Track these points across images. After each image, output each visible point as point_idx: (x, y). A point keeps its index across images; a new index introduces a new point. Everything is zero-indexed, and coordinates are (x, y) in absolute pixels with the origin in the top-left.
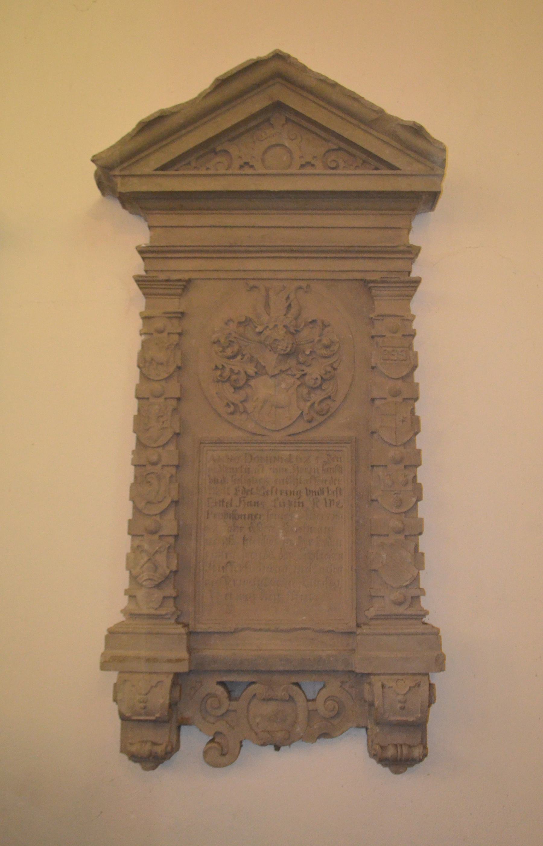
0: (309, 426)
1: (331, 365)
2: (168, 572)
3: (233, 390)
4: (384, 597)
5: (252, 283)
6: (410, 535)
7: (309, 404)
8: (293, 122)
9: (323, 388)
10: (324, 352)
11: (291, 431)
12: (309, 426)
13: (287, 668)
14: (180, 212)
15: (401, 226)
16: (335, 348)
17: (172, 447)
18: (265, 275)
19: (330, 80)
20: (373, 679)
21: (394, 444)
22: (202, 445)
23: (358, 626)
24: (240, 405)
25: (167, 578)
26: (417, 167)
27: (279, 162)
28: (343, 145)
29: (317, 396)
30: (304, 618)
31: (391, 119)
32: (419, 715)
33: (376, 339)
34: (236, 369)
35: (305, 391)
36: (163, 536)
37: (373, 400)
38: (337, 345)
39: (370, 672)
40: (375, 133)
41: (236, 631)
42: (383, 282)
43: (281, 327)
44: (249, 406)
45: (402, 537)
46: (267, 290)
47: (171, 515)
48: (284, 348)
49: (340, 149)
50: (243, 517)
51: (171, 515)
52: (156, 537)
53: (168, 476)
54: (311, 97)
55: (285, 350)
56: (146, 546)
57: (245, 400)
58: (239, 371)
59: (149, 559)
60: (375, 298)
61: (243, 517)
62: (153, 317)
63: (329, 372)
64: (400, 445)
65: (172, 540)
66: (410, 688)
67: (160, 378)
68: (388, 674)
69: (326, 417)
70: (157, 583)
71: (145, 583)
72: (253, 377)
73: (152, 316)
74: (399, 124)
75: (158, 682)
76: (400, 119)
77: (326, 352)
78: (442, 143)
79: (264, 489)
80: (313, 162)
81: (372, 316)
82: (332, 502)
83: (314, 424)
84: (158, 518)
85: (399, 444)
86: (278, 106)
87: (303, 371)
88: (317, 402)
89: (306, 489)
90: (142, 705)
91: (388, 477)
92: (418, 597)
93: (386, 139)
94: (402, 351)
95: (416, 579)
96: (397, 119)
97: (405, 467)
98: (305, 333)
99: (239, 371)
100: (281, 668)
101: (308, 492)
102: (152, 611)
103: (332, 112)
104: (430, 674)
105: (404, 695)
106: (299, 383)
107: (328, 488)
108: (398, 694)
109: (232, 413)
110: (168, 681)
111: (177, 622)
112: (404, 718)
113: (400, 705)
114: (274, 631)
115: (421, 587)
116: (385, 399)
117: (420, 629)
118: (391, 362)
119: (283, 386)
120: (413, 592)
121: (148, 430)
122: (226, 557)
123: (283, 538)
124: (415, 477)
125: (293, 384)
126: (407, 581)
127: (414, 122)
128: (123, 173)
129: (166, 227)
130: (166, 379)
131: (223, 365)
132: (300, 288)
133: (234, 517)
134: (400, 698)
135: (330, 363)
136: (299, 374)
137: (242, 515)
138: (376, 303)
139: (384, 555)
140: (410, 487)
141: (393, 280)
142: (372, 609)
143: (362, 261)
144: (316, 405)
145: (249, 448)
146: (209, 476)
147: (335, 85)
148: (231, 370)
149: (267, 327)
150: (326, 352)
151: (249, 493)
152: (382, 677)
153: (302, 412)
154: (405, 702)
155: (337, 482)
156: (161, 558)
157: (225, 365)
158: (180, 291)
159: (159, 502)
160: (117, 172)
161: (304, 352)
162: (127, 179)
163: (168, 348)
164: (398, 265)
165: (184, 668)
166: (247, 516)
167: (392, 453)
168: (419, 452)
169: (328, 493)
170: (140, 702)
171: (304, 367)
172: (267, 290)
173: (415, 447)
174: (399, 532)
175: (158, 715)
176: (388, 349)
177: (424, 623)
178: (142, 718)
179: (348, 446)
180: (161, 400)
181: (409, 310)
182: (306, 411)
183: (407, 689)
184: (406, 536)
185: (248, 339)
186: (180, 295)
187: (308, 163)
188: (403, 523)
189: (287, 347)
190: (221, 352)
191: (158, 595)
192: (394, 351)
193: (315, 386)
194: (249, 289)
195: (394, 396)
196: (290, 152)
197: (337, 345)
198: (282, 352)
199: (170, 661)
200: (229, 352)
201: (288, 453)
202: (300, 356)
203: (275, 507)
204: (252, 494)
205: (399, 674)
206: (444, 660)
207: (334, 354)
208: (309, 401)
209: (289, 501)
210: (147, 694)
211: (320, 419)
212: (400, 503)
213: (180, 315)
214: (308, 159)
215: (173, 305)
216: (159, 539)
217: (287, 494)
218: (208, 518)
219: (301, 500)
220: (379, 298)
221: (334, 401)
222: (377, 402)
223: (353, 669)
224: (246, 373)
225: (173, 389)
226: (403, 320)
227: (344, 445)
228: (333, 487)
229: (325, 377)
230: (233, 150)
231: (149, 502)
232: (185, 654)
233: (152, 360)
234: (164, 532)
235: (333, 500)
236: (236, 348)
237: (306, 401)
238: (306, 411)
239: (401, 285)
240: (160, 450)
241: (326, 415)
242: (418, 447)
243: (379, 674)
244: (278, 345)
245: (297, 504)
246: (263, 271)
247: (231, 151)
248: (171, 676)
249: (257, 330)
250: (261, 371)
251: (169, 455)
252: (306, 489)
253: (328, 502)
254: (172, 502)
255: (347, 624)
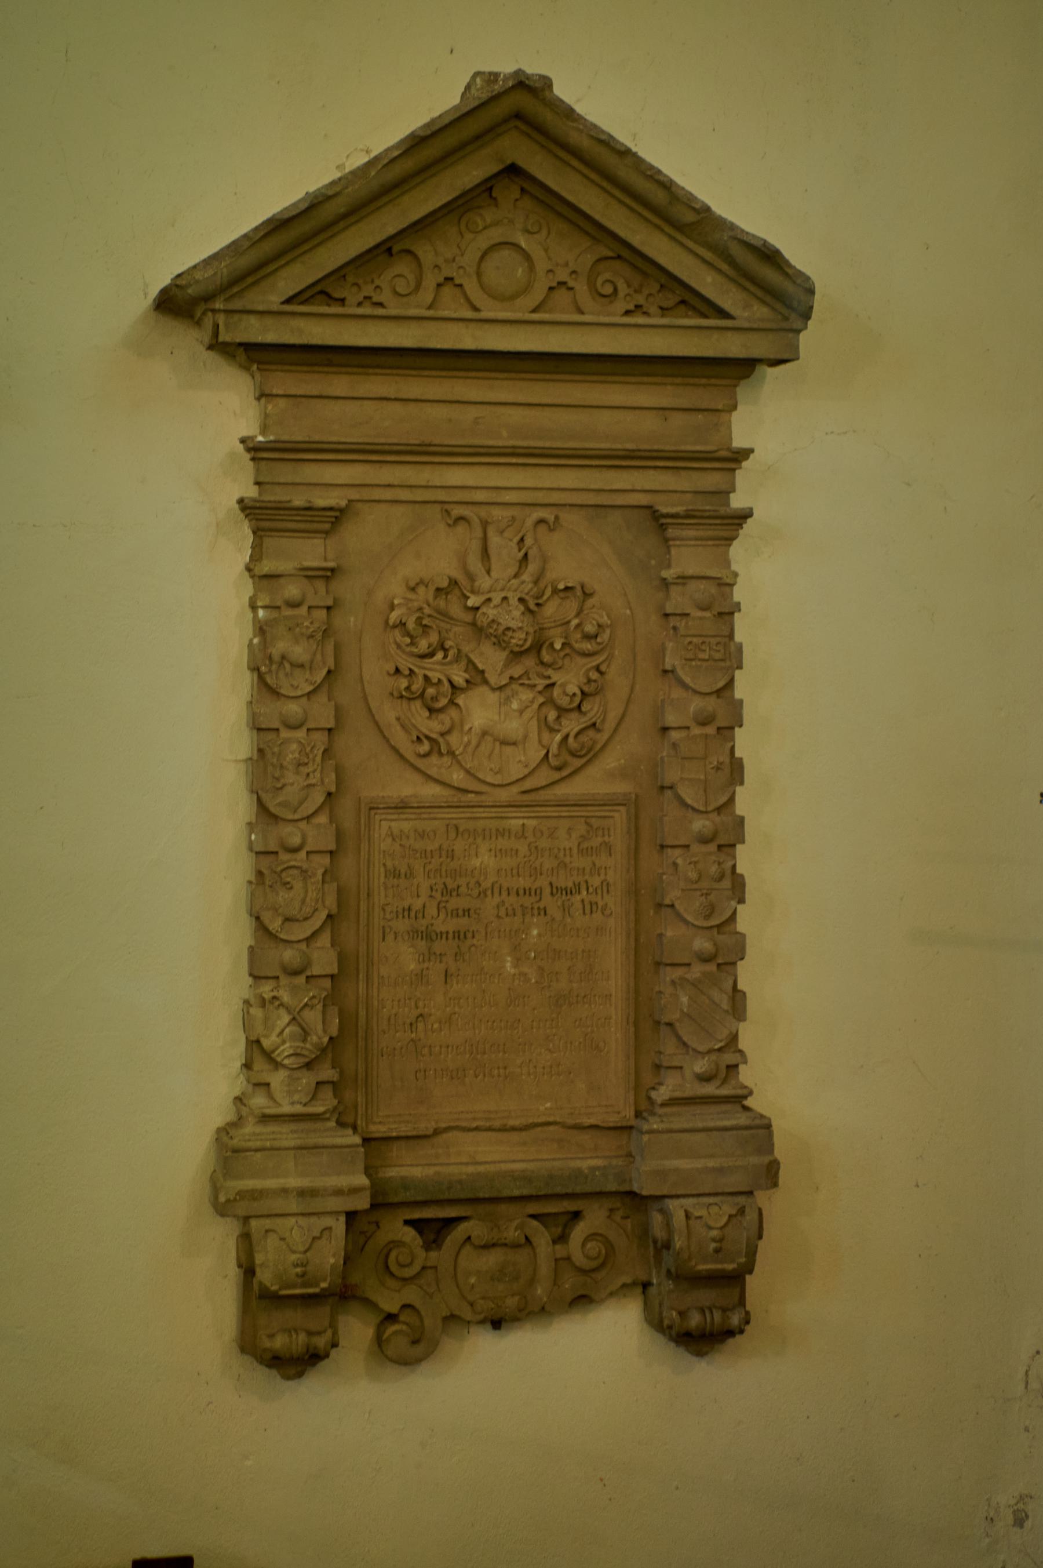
0: (557, 776)
1: (597, 669)
2: (326, 1040)
3: (427, 714)
4: (681, 1068)
5: (457, 511)
6: (726, 964)
7: (558, 737)
8: (530, 194)
9: (583, 709)
10: (587, 646)
11: (528, 785)
12: (557, 776)
13: (525, 1192)
14: (326, 369)
15: (720, 407)
16: (605, 637)
17: (322, 819)
18: (480, 496)
19: (618, 141)
20: (672, 1205)
21: (702, 809)
22: (373, 812)
23: (638, 1114)
24: (441, 740)
25: (324, 1050)
26: (760, 311)
27: (510, 287)
28: (625, 253)
29: (572, 725)
30: (548, 1105)
31: (722, 224)
32: (743, 1260)
33: (673, 621)
34: (434, 676)
35: (552, 715)
36: (313, 976)
37: (665, 729)
38: (608, 631)
39: (665, 1192)
40: (690, 244)
41: (437, 1132)
42: (688, 516)
43: (514, 601)
44: (454, 739)
45: (712, 967)
46: (485, 524)
47: (325, 940)
48: (521, 643)
49: (619, 257)
50: (444, 936)
51: (325, 940)
52: (301, 980)
53: (320, 872)
54: (575, 163)
55: (522, 646)
56: (286, 997)
57: (449, 732)
58: (439, 680)
59: (294, 1019)
60: (671, 543)
61: (444, 936)
62: (279, 576)
63: (595, 681)
64: (713, 811)
65: (327, 983)
66: (730, 1216)
67: (299, 693)
68: (693, 1196)
69: (585, 760)
70: (307, 1060)
71: (286, 1062)
72: (462, 690)
73: (278, 572)
74: (735, 238)
75: (325, 1229)
76: (738, 227)
77: (589, 646)
78: (808, 278)
79: (480, 885)
80: (571, 284)
81: (665, 574)
82: (594, 907)
83: (565, 773)
84: (303, 946)
85: (710, 809)
86: (513, 170)
87: (549, 677)
88: (572, 734)
89: (551, 884)
90: (299, 1270)
91: (692, 866)
92: (737, 1066)
93: (708, 255)
94: (718, 644)
95: (734, 1038)
96: (732, 227)
97: (720, 847)
98: (550, 609)
99: (439, 680)
100: (517, 1193)
101: (555, 890)
102: (299, 1109)
103: (613, 196)
104: (755, 1193)
105: (722, 1228)
106: (541, 700)
107: (587, 882)
108: (710, 1228)
109: (426, 755)
110: (339, 1226)
111: (341, 1124)
112: (719, 1266)
113: (713, 1245)
114: (499, 1130)
115: (740, 1047)
116: (688, 728)
117: (743, 1119)
118: (699, 663)
119: (515, 705)
120: (729, 1058)
121: (281, 788)
122: (417, 1007)
123: (513, 971)
124: (734, 867)
125: (532, 702)
126: (721, 1041)
127: (765, 241)
128: (231, 306)
129: (295, 396)
130: (309, 694)
131: (410, 670)
132: (541, 521)
133: (429, 936)
134: (714, 1233)
135: (594, 664)
136: (541, 683)
137: (441, 933)
138: (673, 551)
139: (685, 1000)
140: (726, 883)
141: (707, 514)
142: (662, 1089)
143: (652, 472)
144: (571, 740)
145: (453, 816)
146: (384, 865)
147: (625, 153)
148: (426, 678)
149: (489, 600)
150: (589, 646)
151: (454, 894)
152: (683, 1201)
153: (548, 752)
154: (721, 1240)
155: (603, 871)
156: (313, 1017)
157: (416, 670)
158: (327, 526)
159: (306, 919)
160: (219, 305)
161: (552, 645)
162: (236, 317)
163: (311, 636)
164: (711, 480)
165: (362, 1203)
166: (451, 935)
167: (700, 825)
168: (741, 821)
169: (588, 889)
170: (296, 1266)
171: (550, 672)
172: (485, 524)
173: (733, 813)
174: (706, 959)
175: (324, 1285)
176: (695, 640)
177: (746, 1109)
178: (297, 1291)
179: (622, 809)
180: (301, 734)
181: (727, 563)
182: (554, 749)
183: (725, 1219)
184: (719, 965)
185: (451, 618)
186: (327, 533)
187: (562, 284)
188: (715, 944)
189: (526, 640)
190: (407, 645)
191: (307, 1080)
192: (703, 643)
193: (571, 706)
194: (451, 522)
195: (703, 724)
196: (527, 257)
197: (608, 631)
198: (517, 649)
199: (338, 1192)
200: (423, 645)
201: (521, 822)
202: (544, 652)
203: (498, 917)
204: (458, 895)
205: (709, 1195)
206: (779, 1169)
207: (602, 649)
208: (559, 731)
209: (522, 906)
210: (306, 1252)
211: (578, 763)
212: (711, 910)
213: (329, 574)
214: (562, 275)
215: (312, 552)
216: (307, 982)
217: (518, 894)
218: (384, 940)
219: (542, 905)
220: (678, 543)
221: (599, 731)
222: (675, 735)
223: (636, 1188)
224: (450, 682)
225: (322, 714)
226: (719, 585)
227: (615, 808)
228: (596, 881)
229: (586, 689)
230: (426, 252)
231: (287, 919)
232: (363, 1180)
233: (283, 657)
234: (316, 970)
235: (596, 903)
236: (434, 638)
237: (552, 730)
238: (554, 749)
239: (718, 521)
240: (303, 825)
241: (588, 755)
242: (739, 812)
243: (678, 1196)
244: (512, 637)
245: (536, 912)
246: (477, 488)
247: (420, 253)
248: (343, 1219)
249: (470, 603)
250: (477, 677)
251: (319, 834)
252: (551, 884)
253: (587, 908)
254: (330, 916)
255: (619, 1113)
